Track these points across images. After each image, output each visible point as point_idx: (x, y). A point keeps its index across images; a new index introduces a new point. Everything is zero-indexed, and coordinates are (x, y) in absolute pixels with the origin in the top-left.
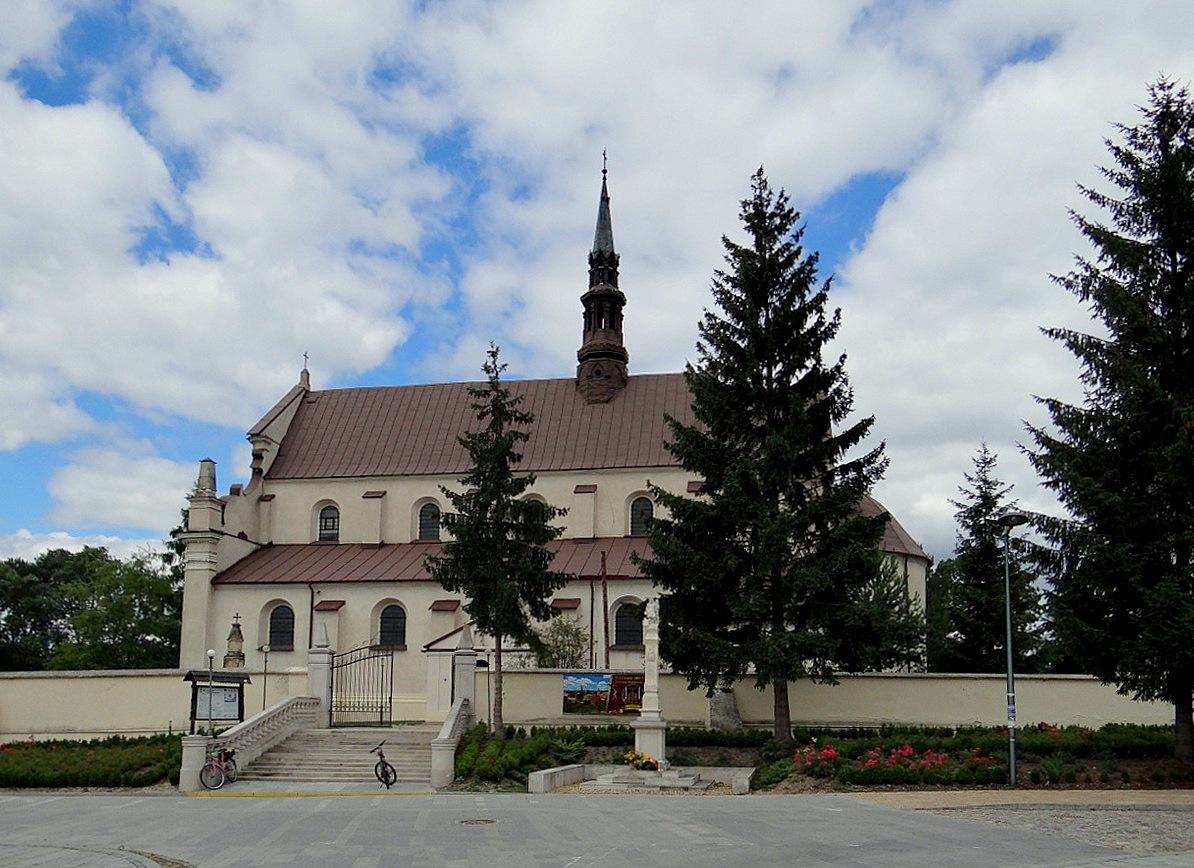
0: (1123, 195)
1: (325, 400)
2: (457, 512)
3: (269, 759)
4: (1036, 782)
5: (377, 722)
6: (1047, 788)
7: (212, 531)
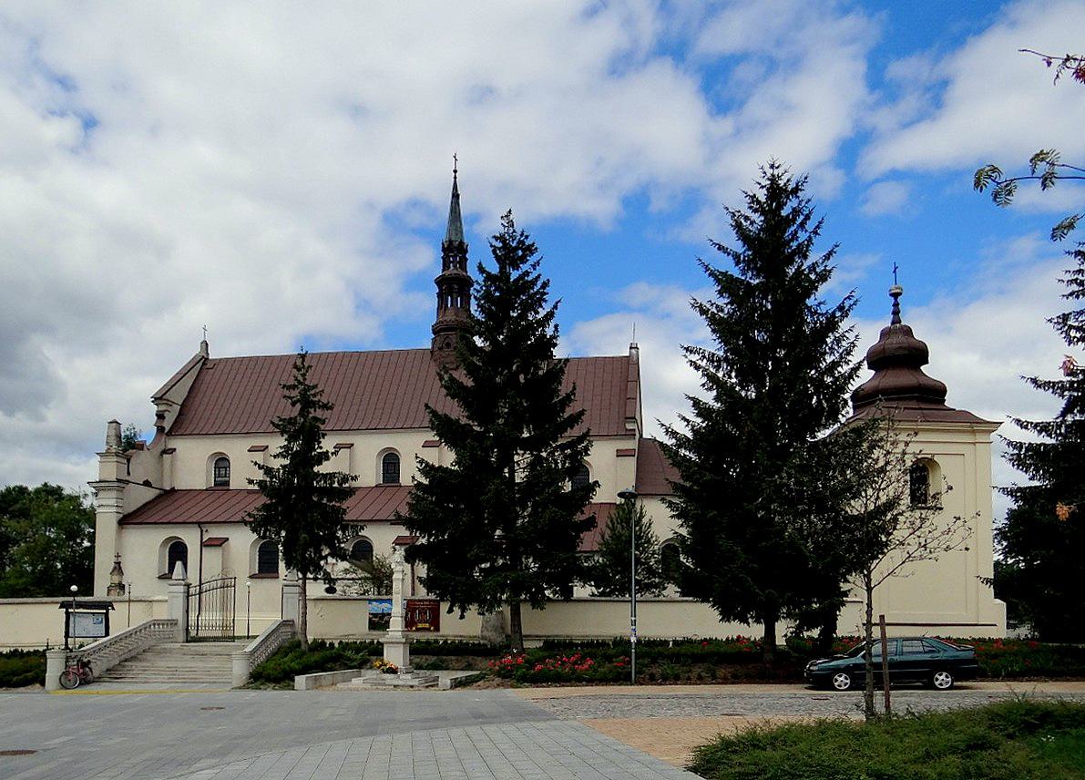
0: (738, 246)
1: (221, 366)
2: (268, 479)
3: (124, 666)
4: (652, 680)
5: (245, 637)
6: (660, 684)
7: (119, 481)
